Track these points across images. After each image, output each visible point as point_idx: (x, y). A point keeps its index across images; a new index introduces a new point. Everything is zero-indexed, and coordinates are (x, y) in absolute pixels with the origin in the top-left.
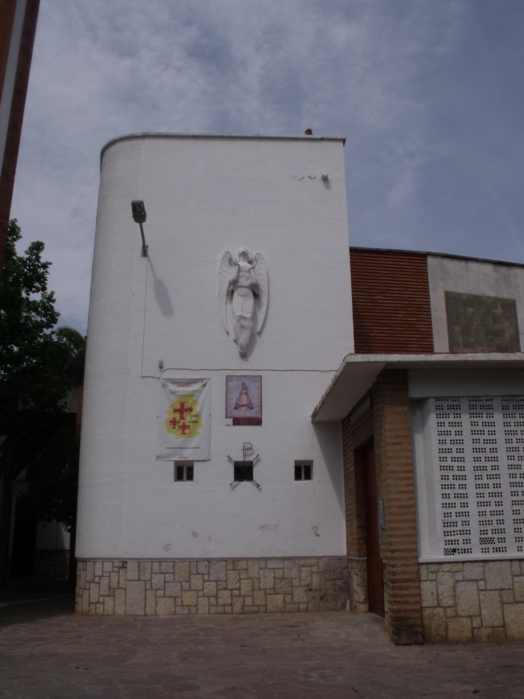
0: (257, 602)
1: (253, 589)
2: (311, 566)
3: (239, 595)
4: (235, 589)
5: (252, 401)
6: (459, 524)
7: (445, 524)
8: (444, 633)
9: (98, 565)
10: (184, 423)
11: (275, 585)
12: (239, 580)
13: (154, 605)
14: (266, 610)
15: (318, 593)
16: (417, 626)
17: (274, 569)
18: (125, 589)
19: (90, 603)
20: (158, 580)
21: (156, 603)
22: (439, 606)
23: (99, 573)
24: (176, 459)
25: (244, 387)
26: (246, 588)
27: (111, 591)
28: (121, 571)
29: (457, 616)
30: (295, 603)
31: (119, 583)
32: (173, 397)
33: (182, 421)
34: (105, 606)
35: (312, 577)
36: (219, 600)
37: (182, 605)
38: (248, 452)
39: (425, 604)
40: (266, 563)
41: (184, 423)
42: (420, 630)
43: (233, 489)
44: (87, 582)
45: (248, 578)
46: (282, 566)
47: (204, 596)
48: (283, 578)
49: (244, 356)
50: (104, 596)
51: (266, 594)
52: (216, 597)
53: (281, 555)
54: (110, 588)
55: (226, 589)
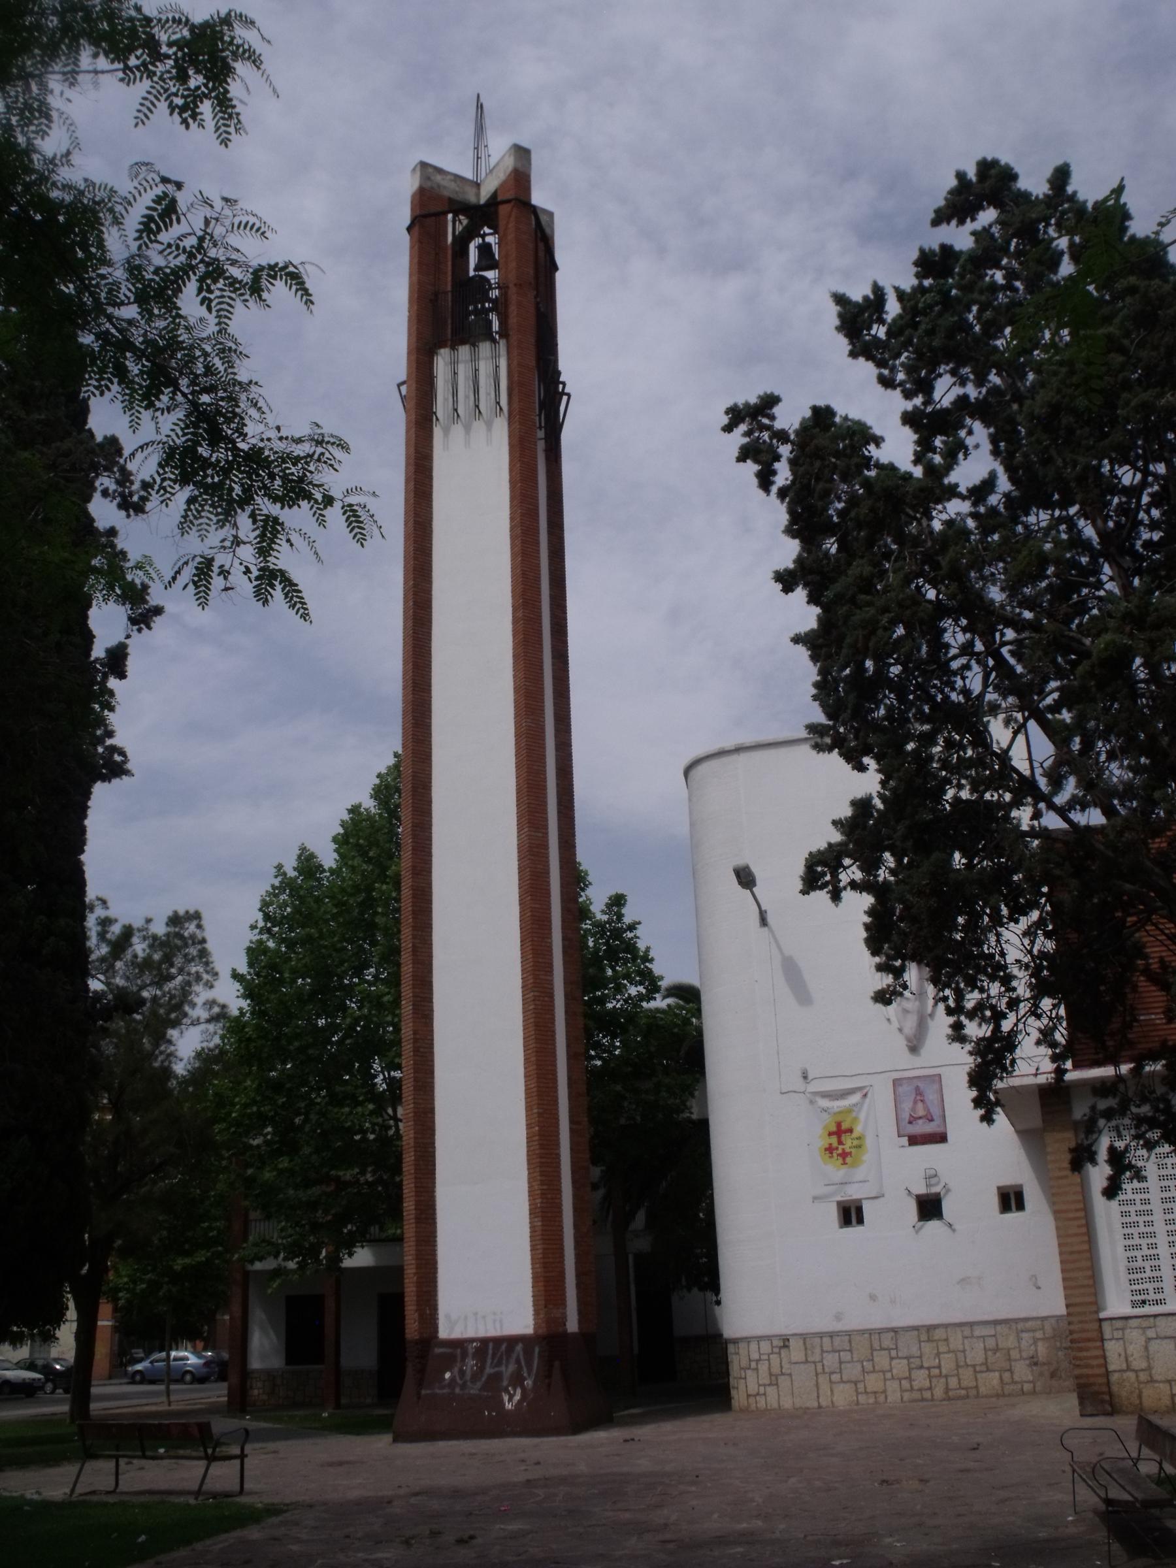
0: (965, 1384)
1: (958, 1367)
2: (1034, 1331)
3: (940, 1375)
4: (934, 1367)
5: (931, 1111)
6: (1148, 1269)
7: (1130, 1271)
8: (1138, 1402)
9: (754, 1346)
10: (843, 1149)
11: (986, 1359)
12: (938, 1354)
13: (829, 1393)
14: (978, 1392)
15: (1046, 1367)
16: (1103, 1393)
17: (983, 1337)
18: (790, 1375)
19: (748, 1396)
20: (830, 1360)
21: (832, 1391)
22: (1129, 1369)
23: (755, 1356)
24: (840, 1199)
25: (919, 1092)
26: (947, 1364)
27: (773, 1378)
28: (784, 1352)
29: (1152, 1381)
30: (1016, 1383)
31: (781, 1367)
32: (825, 1116)
33: (841, 1147)
34: (768, 1399)
35: (1036, 1346)
36: (913, 1383)
37: (866, 1392)
38: (933, 1181)
39: (1111, 1368)
40: (972, 1330)
41: (843, 1149)
42: (1107, 1398)
43: (917, 1232)
44: (741, 1369)
45: (949, 1352)
46: (993, 1333)
47: (893, 1378)
48: (996, 1350)
49: (914, 1049)
50: (765, 1385)
51: (975, 1371)
52: (910, 1379)
53: (991, 1318)
54: (771, 1375)
55: (921, 1367)
